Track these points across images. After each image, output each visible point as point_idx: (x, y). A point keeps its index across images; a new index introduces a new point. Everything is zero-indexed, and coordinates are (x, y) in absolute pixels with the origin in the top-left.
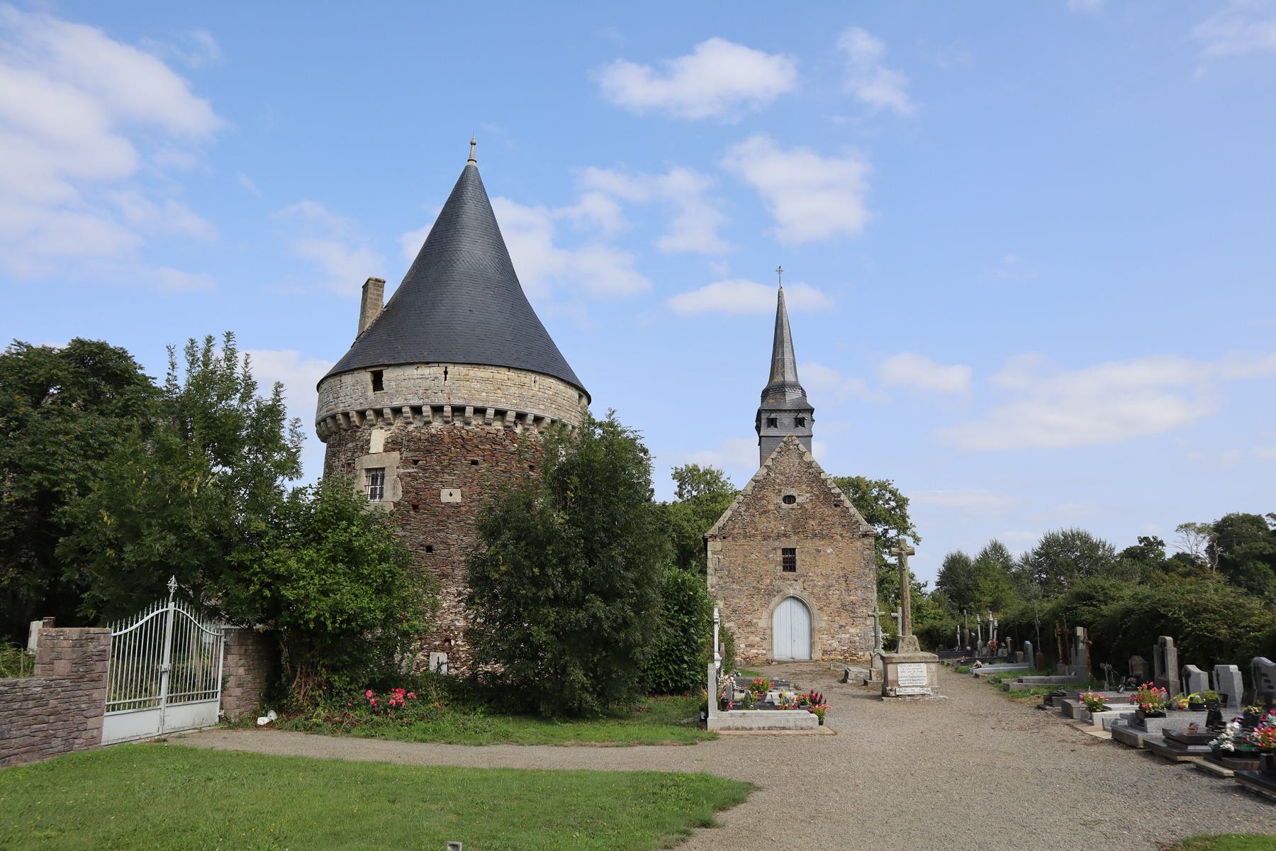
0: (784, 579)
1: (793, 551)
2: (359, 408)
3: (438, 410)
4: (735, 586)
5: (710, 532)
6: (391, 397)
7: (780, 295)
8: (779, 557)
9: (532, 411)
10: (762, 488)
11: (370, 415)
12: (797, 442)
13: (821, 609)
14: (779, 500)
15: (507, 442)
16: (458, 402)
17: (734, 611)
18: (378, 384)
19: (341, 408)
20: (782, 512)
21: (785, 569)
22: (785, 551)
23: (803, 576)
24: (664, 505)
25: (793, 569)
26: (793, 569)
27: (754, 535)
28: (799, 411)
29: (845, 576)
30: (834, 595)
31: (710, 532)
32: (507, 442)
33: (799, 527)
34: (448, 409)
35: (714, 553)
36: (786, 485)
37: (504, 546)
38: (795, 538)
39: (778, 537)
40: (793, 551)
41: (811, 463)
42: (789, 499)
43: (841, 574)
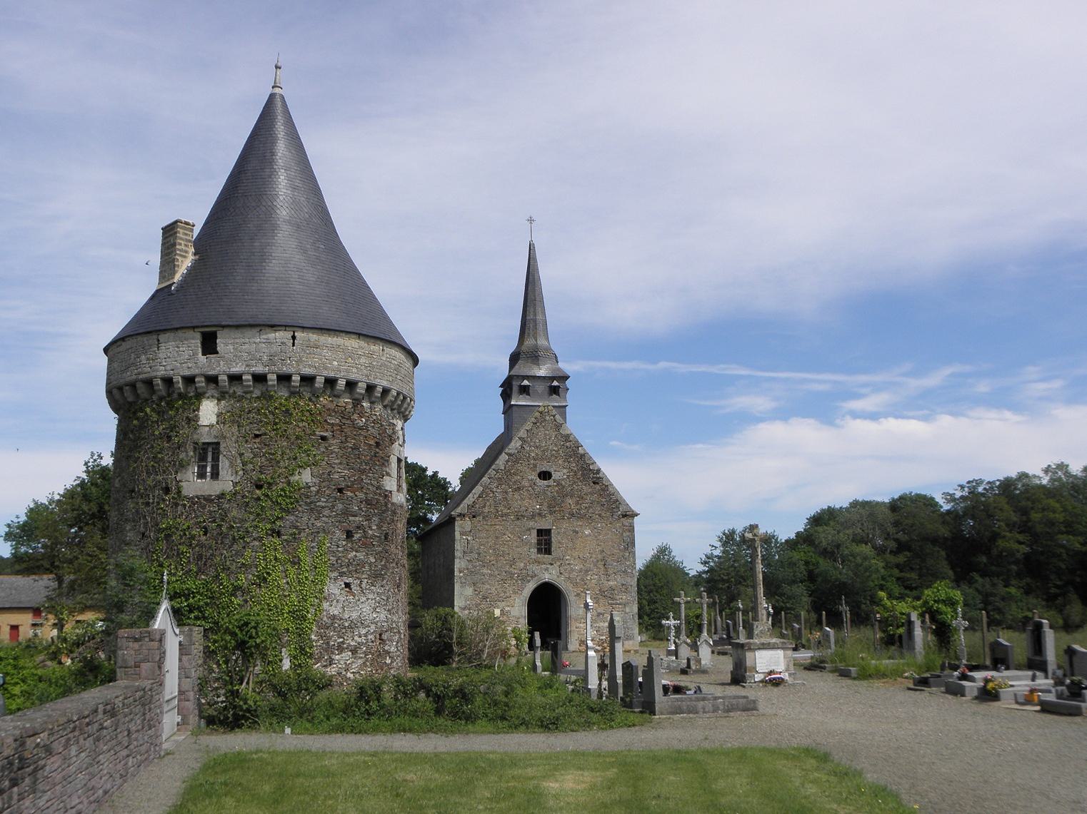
0: (538, 562)
1: (548, 532)
2: (187, 373)
3: (284, 379)
4: (485, 571)
5: (459, 510)
6: (229, 362)
7: (531, 248)
8: (533, 538)
9: (382, 383)
10: (517, 461)
11: (201, 383)
12: (554, 412)
13: (578, 595)
14: (534, 476)
15: (355, 416)
16: (307, 371)
17: (485, 598)
18: (209, 345)
19: (161, 372)
20: (538, 489)
21: (539, 551)
22: (540, 532)
23: (559, 559)
24: (841, 508)
25: (548, 551)
26: (548, 551)
27: (507, 515)
28: (553, 379)
29: (603, 560)
30: (592, 579)
31: (459, 510)
32: (355, 416)
33: (554, 506)
34: (296, 378)
35: (462, 534)
36: (542, 459)
37: (258, 522)
38: (550, 518)
39: (533, 516)
40: (548, 532)
41: (568, 436)
42: (545, 475)
43: (600, 557)
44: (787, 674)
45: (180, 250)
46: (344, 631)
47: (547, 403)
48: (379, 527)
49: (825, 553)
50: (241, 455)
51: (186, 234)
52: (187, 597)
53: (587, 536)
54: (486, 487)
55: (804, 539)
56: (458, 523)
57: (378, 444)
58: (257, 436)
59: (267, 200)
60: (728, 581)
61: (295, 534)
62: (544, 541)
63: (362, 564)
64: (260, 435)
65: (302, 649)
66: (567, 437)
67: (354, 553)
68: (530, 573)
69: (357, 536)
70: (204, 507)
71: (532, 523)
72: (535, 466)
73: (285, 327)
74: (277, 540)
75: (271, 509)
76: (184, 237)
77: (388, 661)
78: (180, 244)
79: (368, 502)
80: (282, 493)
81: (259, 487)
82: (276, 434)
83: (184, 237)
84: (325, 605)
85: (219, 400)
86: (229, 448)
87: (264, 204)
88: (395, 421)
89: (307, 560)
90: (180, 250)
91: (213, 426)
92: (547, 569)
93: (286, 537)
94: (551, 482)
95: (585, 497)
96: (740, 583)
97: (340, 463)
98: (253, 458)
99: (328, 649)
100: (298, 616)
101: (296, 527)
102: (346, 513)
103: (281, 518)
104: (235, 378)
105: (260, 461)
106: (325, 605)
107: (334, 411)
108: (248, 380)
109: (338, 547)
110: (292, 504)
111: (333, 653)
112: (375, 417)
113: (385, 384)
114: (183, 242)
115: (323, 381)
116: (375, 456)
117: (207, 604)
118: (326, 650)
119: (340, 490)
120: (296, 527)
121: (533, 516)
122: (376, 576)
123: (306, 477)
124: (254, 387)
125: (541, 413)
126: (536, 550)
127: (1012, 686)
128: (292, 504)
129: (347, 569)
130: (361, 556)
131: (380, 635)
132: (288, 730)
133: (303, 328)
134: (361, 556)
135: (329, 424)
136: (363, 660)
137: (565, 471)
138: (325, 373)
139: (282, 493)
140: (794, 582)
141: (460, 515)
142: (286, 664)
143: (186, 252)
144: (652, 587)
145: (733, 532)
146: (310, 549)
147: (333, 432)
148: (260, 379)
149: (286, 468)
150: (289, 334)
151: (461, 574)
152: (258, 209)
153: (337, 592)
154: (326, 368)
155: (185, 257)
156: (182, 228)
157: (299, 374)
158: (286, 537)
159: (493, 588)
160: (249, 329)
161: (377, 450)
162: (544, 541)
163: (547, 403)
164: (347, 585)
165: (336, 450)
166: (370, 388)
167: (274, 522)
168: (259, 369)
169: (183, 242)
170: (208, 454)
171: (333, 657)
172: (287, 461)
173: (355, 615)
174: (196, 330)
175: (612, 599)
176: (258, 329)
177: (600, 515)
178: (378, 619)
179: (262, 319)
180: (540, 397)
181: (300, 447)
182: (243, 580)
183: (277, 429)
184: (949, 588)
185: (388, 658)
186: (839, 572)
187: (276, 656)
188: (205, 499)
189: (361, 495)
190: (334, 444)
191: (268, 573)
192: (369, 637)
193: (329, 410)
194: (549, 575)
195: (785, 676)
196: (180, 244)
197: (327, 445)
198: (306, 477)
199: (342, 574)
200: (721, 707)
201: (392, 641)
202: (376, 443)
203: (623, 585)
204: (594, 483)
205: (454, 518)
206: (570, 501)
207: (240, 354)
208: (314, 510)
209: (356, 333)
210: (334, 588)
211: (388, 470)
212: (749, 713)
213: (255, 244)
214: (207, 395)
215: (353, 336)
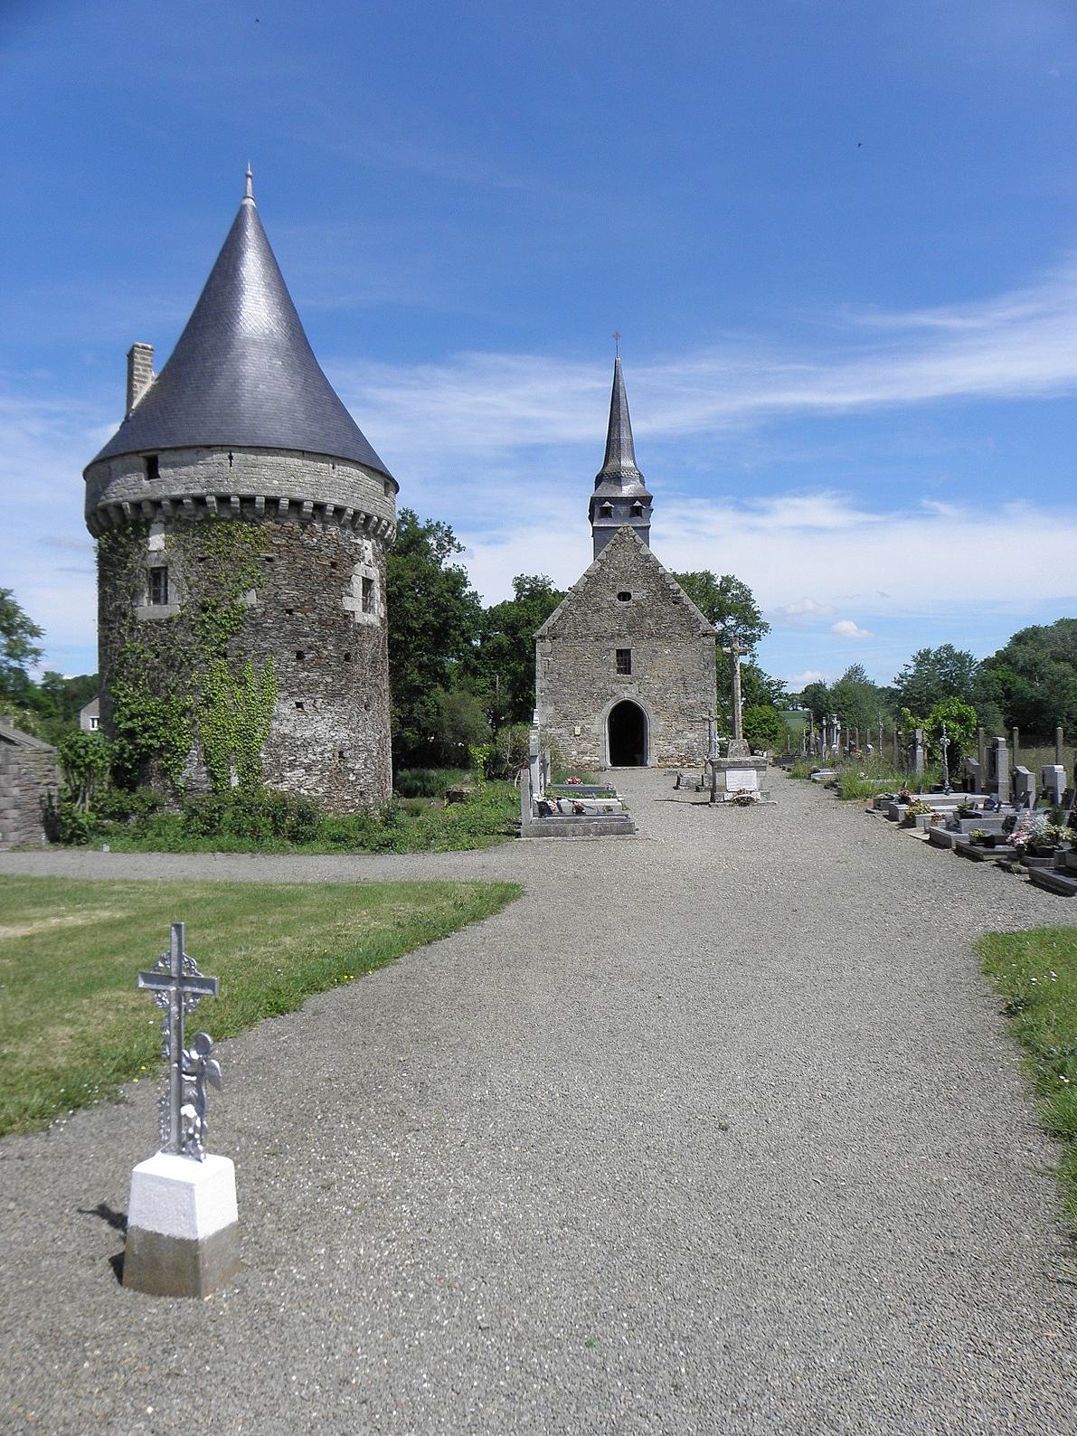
5: (539, 632)
11: (147, 509)
14: (613, 597)
15: (305, 536)
16: (246, 491)
18: (152, 472)
22: (620, 653)
23: (638, 678)
27: (587, 635)
31: (539, 632)
32: (305, 536)
33: (633, 628)
36: (622, 581)
39: (612, 637)
41: (648, 556)
42: (624, 596)
44: (759, 794)
45: (137, 376)
46: (296, 749)
47: (626, 524)
48: (337, 646)
49: (1022, 671)
50: (187, 578)
51: (144, 359)
52: (143, 717)
53: (666, 655)
54: (565, 610)
55: (1004, 658)
56: (539, 645)
57: (334, 565)
58: (201, 560)
59: (225, 318)
60: (919, 700)
61: (241, 656)
62: (624, 658)
63: (317, 684)
64: (205, 558)
65: (249, 767)
66: (647, 558)
67: (306, 673)
68: (609, 692)
69: (308, 657)
70: (155, 631)
71: (611, 644)
72: (614, 587)
73: (222, 448)
74: (222, 662)
75: (217, 631)
76: (142, 362)
77: (352, 778)
78: (138, 369)
79: (322, 623)
80: (227, 615)
81: (205, 610)
82: (220, 557)
83: (142, 362)
84: (275, 724)
85: (166, 524)
86: (176, 573)
87: (221, 321)
88: (359, 541)
89: (254, 682)
90: (137, 376)
91: (160, 551)
92: (626, 688)
93: (231, 659)
94: (630, 603)
95: (665, 617)
96: (932, 702)
97: (288, 584)
98: (198, 581)
99: (278, 766)
100: (246, 735)
101: (242, 649)
102: (297, 633)
103: (226, 641)
104: (177, 502)
105: (204, 584)
106: (275, 724)
107: (279, 532)
108: (236, 503)
109: (287, 667)
110: (236, 625)
111: (283, 770)
112: (329, 537)
113: (355, 506)
114: (140, 367)
115: (264, 501)
116: (331, 577)
117: (160, 724)
118: (276, 767)
119: (290, 612)
120: (242, 649)
121: (612, 637)
122: (333, 695)
123: (251, 598)
124: (197, 510)
125: (620, 534)
126: (616, 670)
127: (934, 811)
128: (236, 625)
129: (299, 692)
130: (314, 676)
131: (341, 753)
132: (106, 848)
133: (240, 448)
134: (314, 676)
135: (275, 545)
136: (319, 777)
137: (645, 591)
138: (265, 493)
139: (227, 615)
140: (987, 700)
141: (540, 637)
142: (235, 782)
143: (145, 377)
144: (841, 706)
145: (928, 652)
146: (257, 671)
147: (279, 553)
148: (200, 501)
149: (230, 590)
150: (226, 456)
151: (543, 694)
152: (216, 328)
153: (287, 711)
154: (265, 488)
155: (144, 382)
156: (139, 353)
157: (238, 495)
158: (231, 659)
159: (572, 707)
160: (173, 452)
161: (333, 570)
162: (624, 658)
163: (626, 524)
164: (299, 705)
165: (283, 571)
166: (319, 507)
167: (219, 645)
168: (198, 491)
169: (140, 367)
170: (158, 577)
171: (284, 774)
172: (231, 584)
173: (307, 734)
174: (140, 455)
175: (692, 717)
176: (195, 450)
177: (679, 635)
178: (337, 738)
179: (200, 441)
180: (623, 519)
181: (244, 570)
182: (190, 700)
183: (220, 552)
184: (962, 703)
185: (351, 775)
186: (1036, 690)
187: (224, 773)
188: (156, 623)
189: (314, 616)
190: (281, 566)
191: (214, 694)
192: (326, 755)
193: (274, 531)
194: (629, 693)
195: (757, 795)
196: (138, 369)
197: (273, 566)
198: (251, 598)
199: (292, 694)
200: (593, 830)
201: (357, 759)
202: (332, 563)
203: (702, 703)
204: (674, 603)
205: (535, 640)
206: (649, 622)
207: (177, 481)
208: (258, 628)
209: (300, 451)
210: (285, 708)
211: (348, 590)
212: (621, 837)
213: (207, 364)
214: (156, 520)
215: (297, 454)
